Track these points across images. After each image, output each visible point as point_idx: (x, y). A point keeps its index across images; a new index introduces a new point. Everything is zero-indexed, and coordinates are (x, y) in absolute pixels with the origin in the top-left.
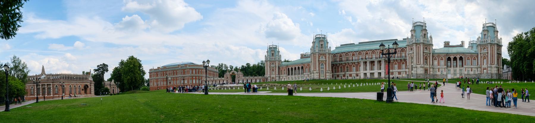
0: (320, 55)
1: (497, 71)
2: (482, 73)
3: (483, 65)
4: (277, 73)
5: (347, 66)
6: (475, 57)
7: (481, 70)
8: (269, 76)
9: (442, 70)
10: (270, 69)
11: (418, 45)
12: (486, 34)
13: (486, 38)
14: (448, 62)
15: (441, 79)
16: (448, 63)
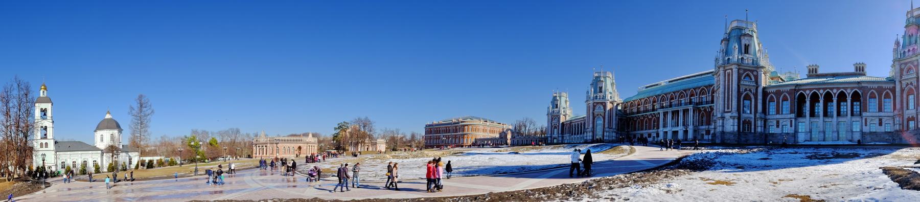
0: (595, 104)
1: (763, 128)
2: (905, 128)
3: (908, 109)
4: (560, 132)
5: (646, 120)
6: (887, 93)
7: (901, 123)
8: (549, 135)
9: (784, 123)
10: (739, 93)
11: (728, 71)
12: (912, 35)
13: (914, 42)
14: (855, 103)
15: (171, 176)
16: (855, 107)
